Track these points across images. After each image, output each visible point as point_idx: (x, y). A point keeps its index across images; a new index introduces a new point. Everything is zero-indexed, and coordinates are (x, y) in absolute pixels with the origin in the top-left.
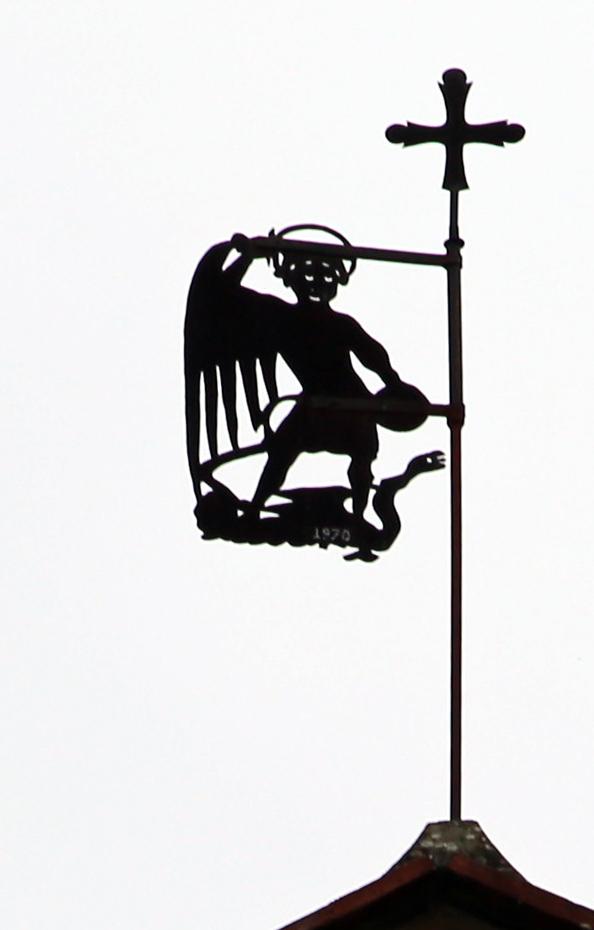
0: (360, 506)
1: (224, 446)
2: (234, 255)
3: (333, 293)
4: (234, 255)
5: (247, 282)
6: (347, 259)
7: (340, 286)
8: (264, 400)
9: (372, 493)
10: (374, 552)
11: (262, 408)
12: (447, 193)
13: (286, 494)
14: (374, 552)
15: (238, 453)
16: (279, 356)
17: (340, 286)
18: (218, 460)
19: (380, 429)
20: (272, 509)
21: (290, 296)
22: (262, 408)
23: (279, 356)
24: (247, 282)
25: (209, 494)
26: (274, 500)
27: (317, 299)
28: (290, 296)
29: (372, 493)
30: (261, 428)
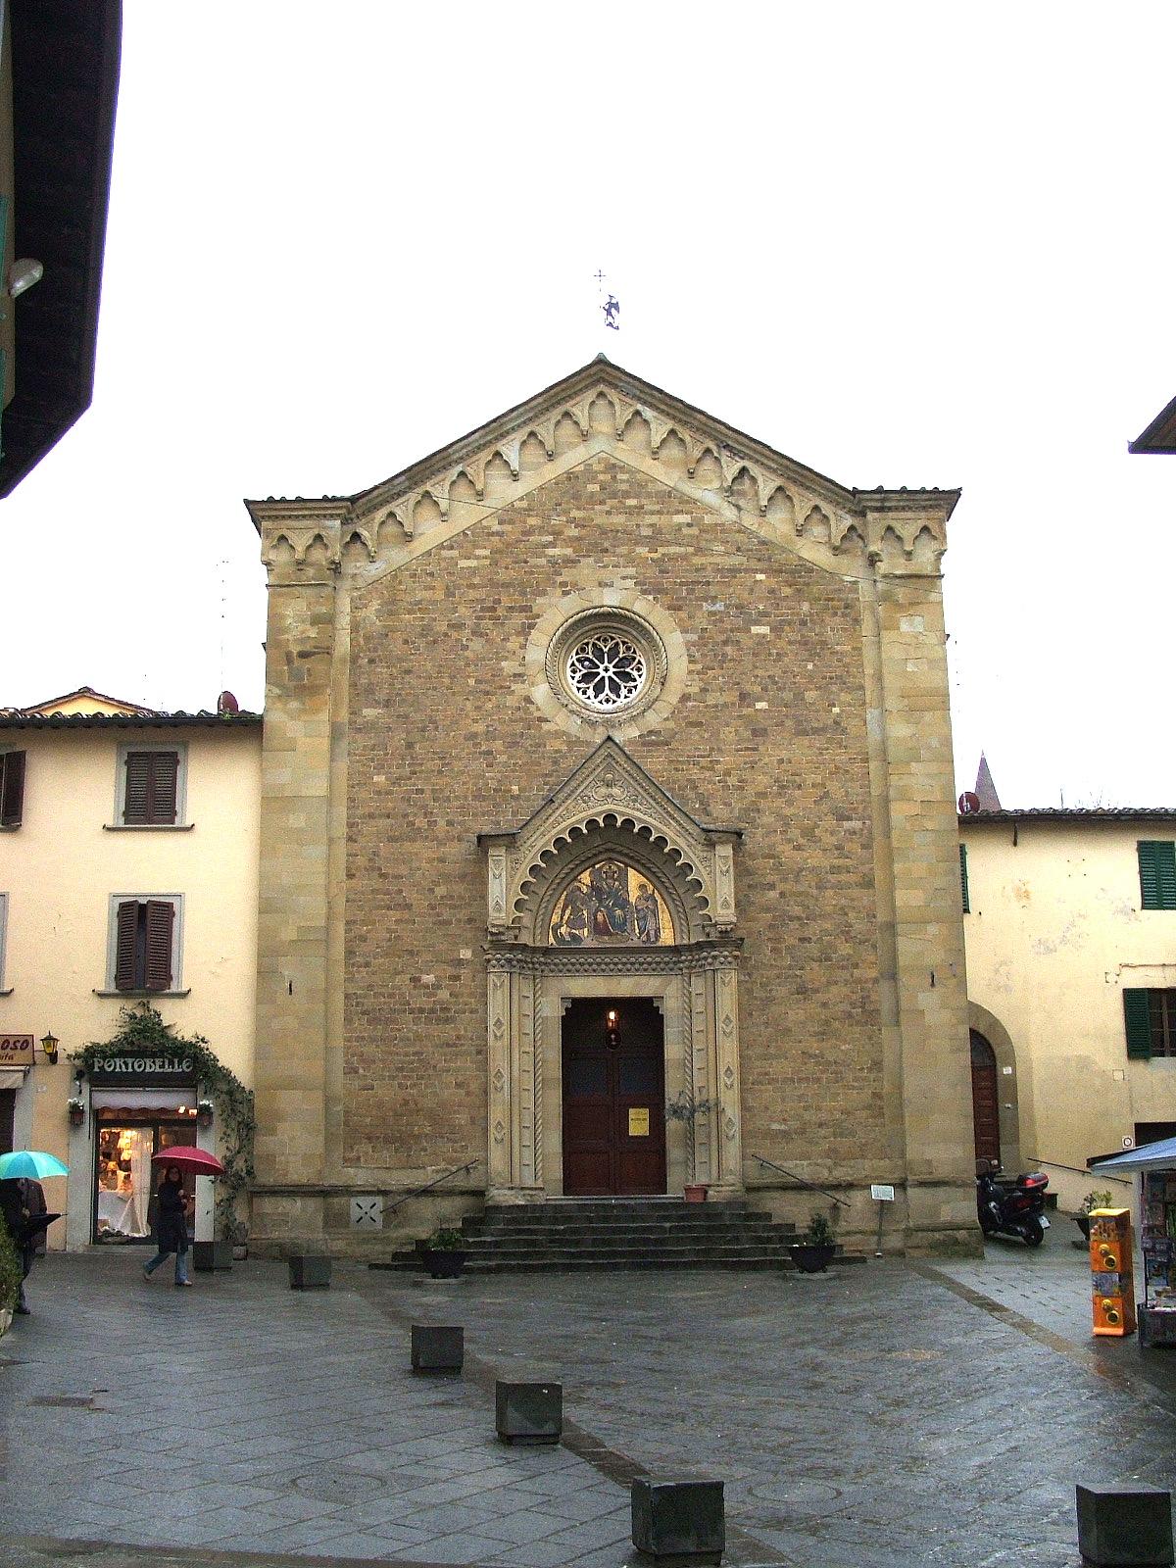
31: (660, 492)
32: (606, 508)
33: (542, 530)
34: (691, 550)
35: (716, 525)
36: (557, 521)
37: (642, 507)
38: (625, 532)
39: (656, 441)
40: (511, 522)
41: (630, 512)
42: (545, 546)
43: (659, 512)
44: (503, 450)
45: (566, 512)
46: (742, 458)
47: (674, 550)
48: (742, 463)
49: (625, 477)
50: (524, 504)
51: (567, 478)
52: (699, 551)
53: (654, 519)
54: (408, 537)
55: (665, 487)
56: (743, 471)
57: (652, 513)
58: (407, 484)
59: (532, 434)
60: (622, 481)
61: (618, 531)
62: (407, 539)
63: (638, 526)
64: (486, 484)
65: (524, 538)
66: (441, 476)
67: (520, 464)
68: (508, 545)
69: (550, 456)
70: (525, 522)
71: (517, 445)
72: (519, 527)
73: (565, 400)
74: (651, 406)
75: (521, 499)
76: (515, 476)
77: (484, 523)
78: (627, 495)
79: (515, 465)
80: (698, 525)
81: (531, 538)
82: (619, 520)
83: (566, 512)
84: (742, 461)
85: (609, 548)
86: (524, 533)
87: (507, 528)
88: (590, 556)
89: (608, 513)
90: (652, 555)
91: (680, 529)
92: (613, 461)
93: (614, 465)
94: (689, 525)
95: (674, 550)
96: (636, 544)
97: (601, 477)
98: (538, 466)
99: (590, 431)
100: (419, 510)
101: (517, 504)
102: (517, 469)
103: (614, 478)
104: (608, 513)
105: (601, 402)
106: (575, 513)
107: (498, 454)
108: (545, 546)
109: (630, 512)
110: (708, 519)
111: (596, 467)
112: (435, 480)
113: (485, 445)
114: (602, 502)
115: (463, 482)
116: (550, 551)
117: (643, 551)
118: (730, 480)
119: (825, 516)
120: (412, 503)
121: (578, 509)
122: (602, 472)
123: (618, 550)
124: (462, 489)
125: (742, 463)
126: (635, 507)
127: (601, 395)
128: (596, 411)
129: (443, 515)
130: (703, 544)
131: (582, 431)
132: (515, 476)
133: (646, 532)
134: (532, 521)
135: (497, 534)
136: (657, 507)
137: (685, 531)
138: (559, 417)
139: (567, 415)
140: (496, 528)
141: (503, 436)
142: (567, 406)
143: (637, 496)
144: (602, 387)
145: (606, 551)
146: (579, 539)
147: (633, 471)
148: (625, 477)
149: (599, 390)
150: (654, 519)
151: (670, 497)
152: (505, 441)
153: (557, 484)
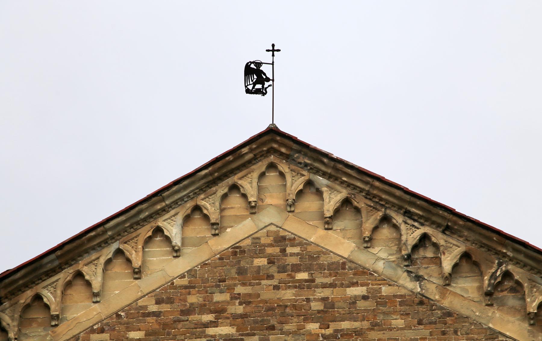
0: (263, 90)
1: (248, 84)
2: (250, 63)
4: (250, 63)
5: (251, 66)
8: (253, 79)
13: (255, 89)
18: (248, 85)
19: (265, 82)
20: (254, 90)
21: (255, 68)
24: (251, 66)
28: (255, 68)
31: (333, 263)
32: (275, 282)
33: (203, 309)
34: (366, 324)
35: (395, 296)
36: (218, 297)
37: (313, 281)
38: (294, 307)
39: (329, 212)
40: (170, 301)
41: (300, 285)
42: (207, 325)
43: (332, 285)
44: (85, 270)
45: (230, 289)
46: (422, 224)
47: (345, 325)
48: (423, 230)
49: (296, 250)
50: (185, 282)
51: (232, 252)
52: (374, 326)
53: (326, 293)
54: (137, 273)
55: (339, 258)
56: (425, 237)
57: (324, 286)
58: (57, 263)
59: (119, 252)
60: (292, 255)
61: (286, 306)
62: (136, 276)
63: (308, 300)
64: (144, 262)
65: (183, 318)
66: (94, 256)
67: (183, 240)
68: (165, 326)
69: (253, 207)
70: (185, 300)
71: (179, 219)
72: (178, 306)
73: (233, 172)
74: (324, 174)
75: (182, 276)
76: (176, 252)
77: (141, 303)
78: (297, 268)
79: (177, 241)
80: (374, 297)
81: (191, 318)
82: (288, 295)
83: (230, 289)
84: (422, 228)
85: (277, 325)
86: (184, 312)
87: (165, 308)
88: (254, 335)
89: (276, 288)
90: (323, 331)
91: (354, 303)
92: (282, 233)
93: (284, 238)
94: (365, 298)
95: (345, 325)
96: (306, 320)
97: (269, 250)
98: (203, 241)
99: (260, 203)
100: (69, 292)
101: (177, 282)
102: (179, 244)
103: (283, 251)
104: (276, 288)
105: (272, 175)
106: (240, 289)
107: (159, 230)
108: (207, 325)
109: (300, 285)
110: (385, 290)
111: (263, 241)
112: (87, 258)
113: (220, 179)
114: (270, 277)
115: (119, 261)
116: (211, 331)
117: (313, 327)
118: (410, 248)
119: (518, 283)
120: (61, 283)
121: (244, 284)
122: (271, 245)
123: (287, 327)
124: (118, 267)
125: (423, 230)
126: (306, 281)
127: (272, 166)
128: (266, 183)
129: (96, 295)
130: (380, 318)
131: (173, 247)
132: (176, 251)
133: (316, 306)
134: (193, 299)
135: (156, 314)
136: (329, 280)
137: (361, 304)
138: (226, 190)
139: (234, 188)
140: (153, 308)
141: (164, 210)
142: (234, 179)
143: (308, 269)
144: (272, 158)
145: (273, 328)
146: (243, 316)
147: (304, 244)
148: (296, 250)
149: (270, 161)
150: (326, 293)
151: (344, 268)
152: (167, 216)
153: (220, 259)
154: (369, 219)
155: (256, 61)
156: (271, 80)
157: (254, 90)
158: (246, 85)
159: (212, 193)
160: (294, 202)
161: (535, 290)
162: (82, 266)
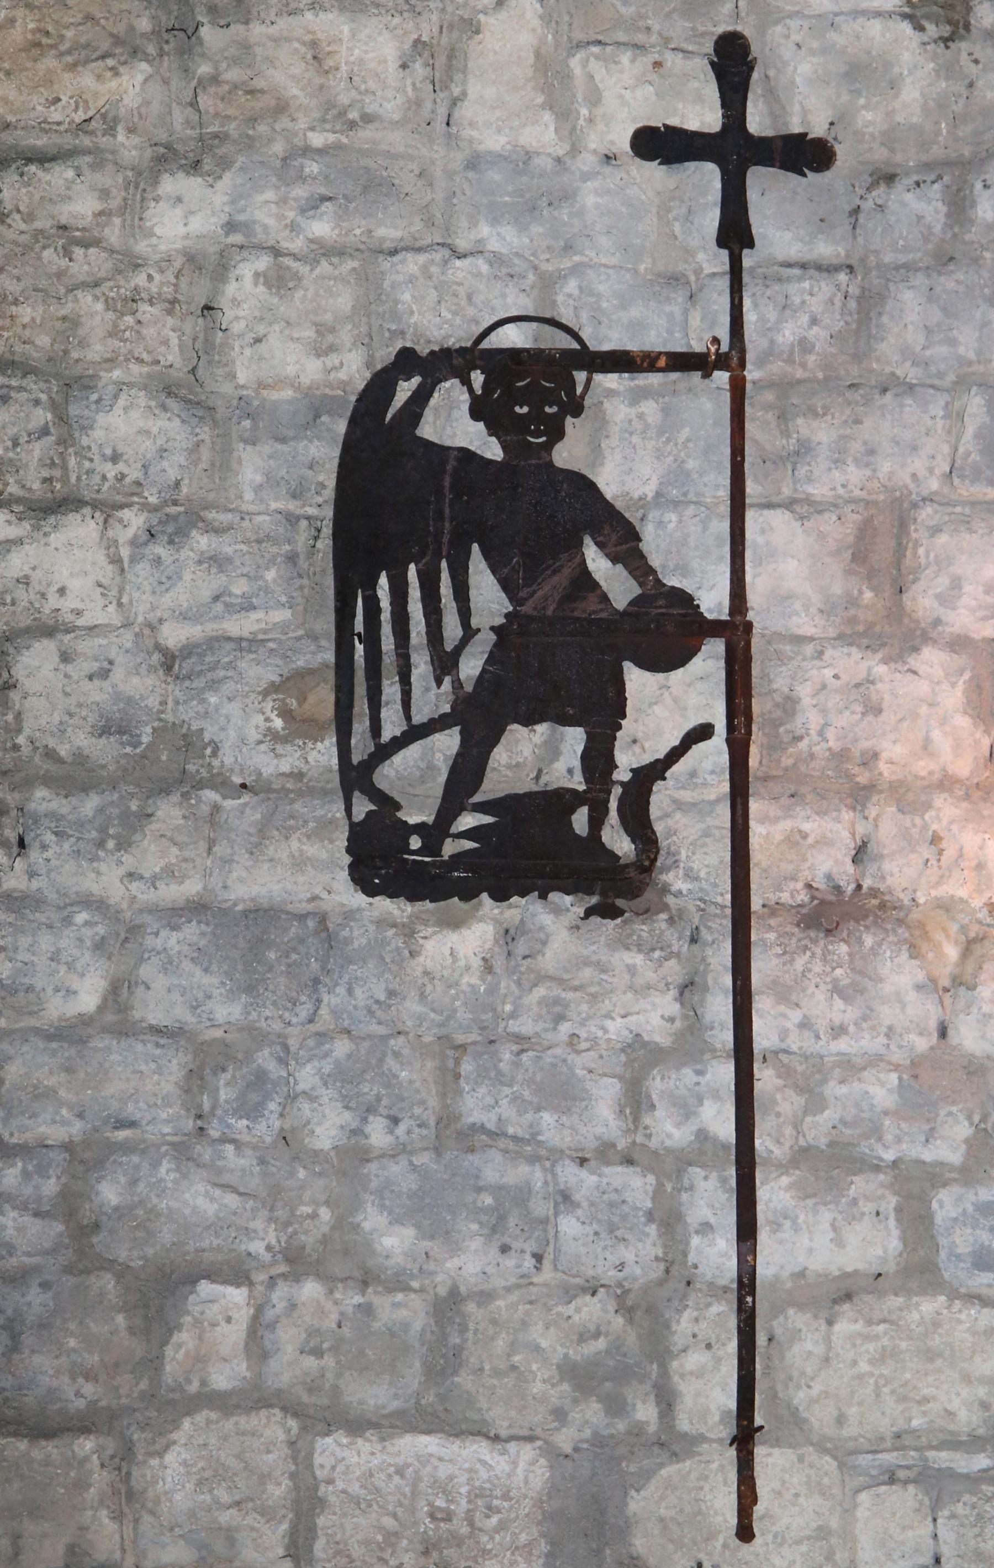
0: (597, 822)
1: (392, 726)
2: (405, 390)
3: (557, 433)
4: (405, 390)
5: (428, 430)
6: (581, 368)
7: (569, 420)
8: (452, 629)
9: (617, 791)
10: (806, 170)
11: (449, 647)
12: (725, 254)
13: (481, 808)
14: (806, 170)
15: (415, 733)
16: (475, 547)
17: (569, 420)
18: (384, 752)
19: (575, 373)
20: (467, 835)
21: (493, 450)
22: (449, 647)
23: (475, 547)
24: (428, 430)
25: (370, 814)
26: (467, 821)
27: (525, 410)
28: (493, 450)
29: (617, 791)
30: (447, 680)
154: (644, 1485)
155: (494, 342)
156: (715, 628)
157: (467, 821)
158: (361, 747)
159: (437, 1441)
160: (63, 48)
161: (624, 1464)
162: (904, 1436)
